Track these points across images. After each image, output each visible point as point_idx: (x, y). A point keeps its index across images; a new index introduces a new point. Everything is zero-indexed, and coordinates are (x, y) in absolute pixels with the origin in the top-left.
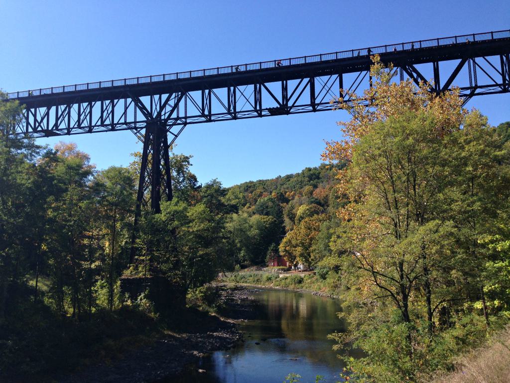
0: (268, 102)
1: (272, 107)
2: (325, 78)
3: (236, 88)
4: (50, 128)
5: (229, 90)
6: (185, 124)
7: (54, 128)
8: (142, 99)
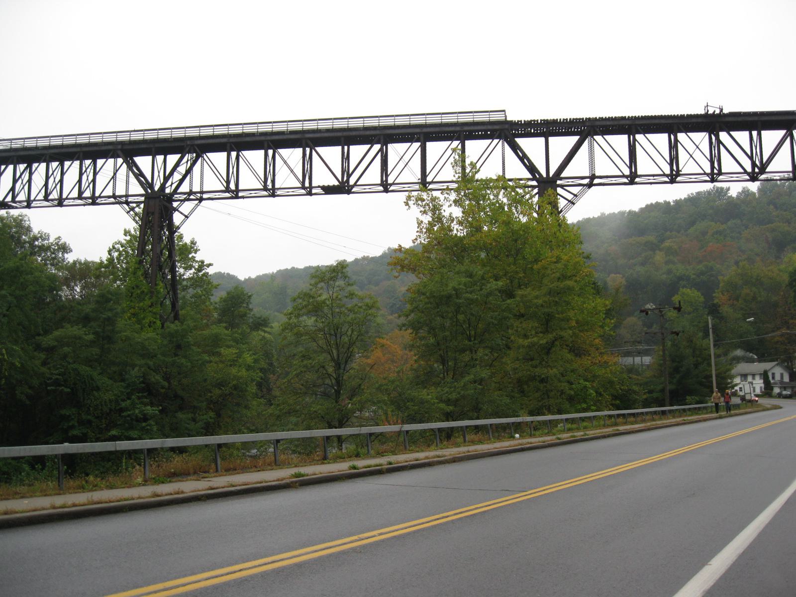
0: (322, 177)
1: (326, 185)
5: (266, 155)
6: (201, 200)
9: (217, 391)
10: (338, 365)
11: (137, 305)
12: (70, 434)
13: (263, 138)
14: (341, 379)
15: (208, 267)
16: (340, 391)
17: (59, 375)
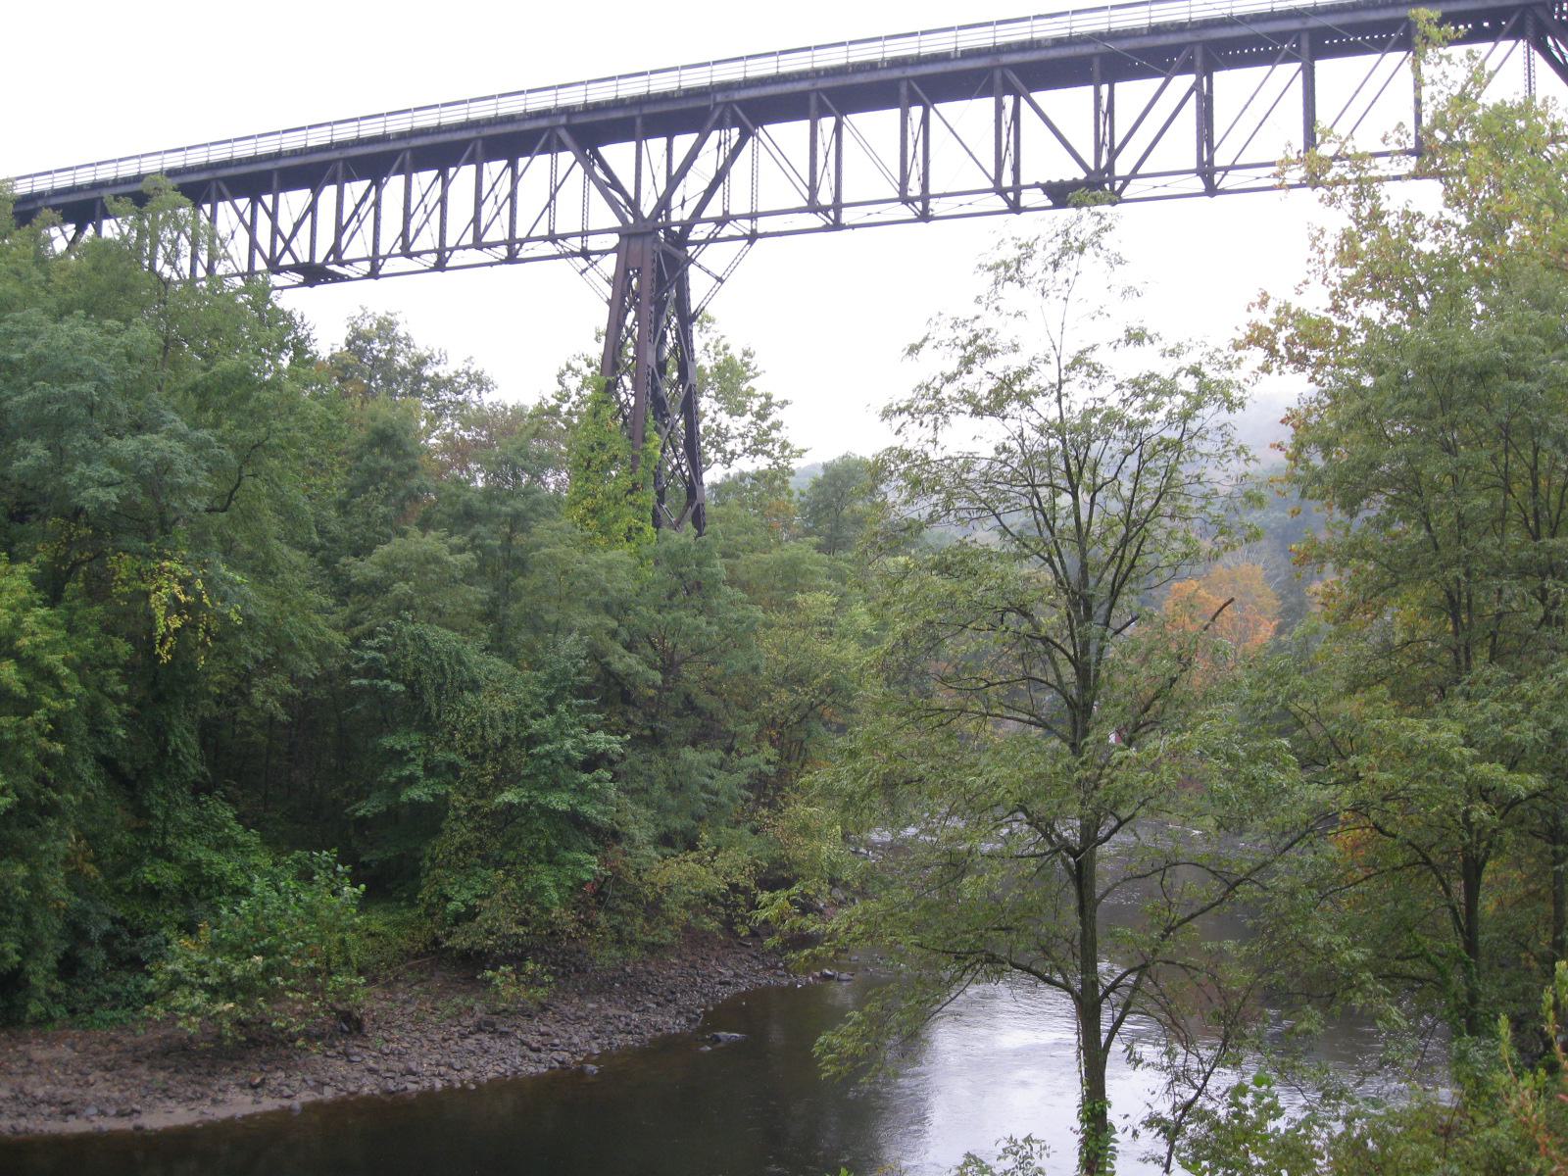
1: (1055, 179)
2: (1252, 75)
3: (932, 111)
4: (319, 259)
5: (999, 108)
6: (752, 237)
7: (331, 259)
8: (607, 152)
9: (784, 696)
10: (1081, 604)
11: (601, 489)
12: (404, 798)
13: (896, 74)
14: (1094, 659)
15: (782, 407)
16: (1087, 710)
17: (380, 649)
